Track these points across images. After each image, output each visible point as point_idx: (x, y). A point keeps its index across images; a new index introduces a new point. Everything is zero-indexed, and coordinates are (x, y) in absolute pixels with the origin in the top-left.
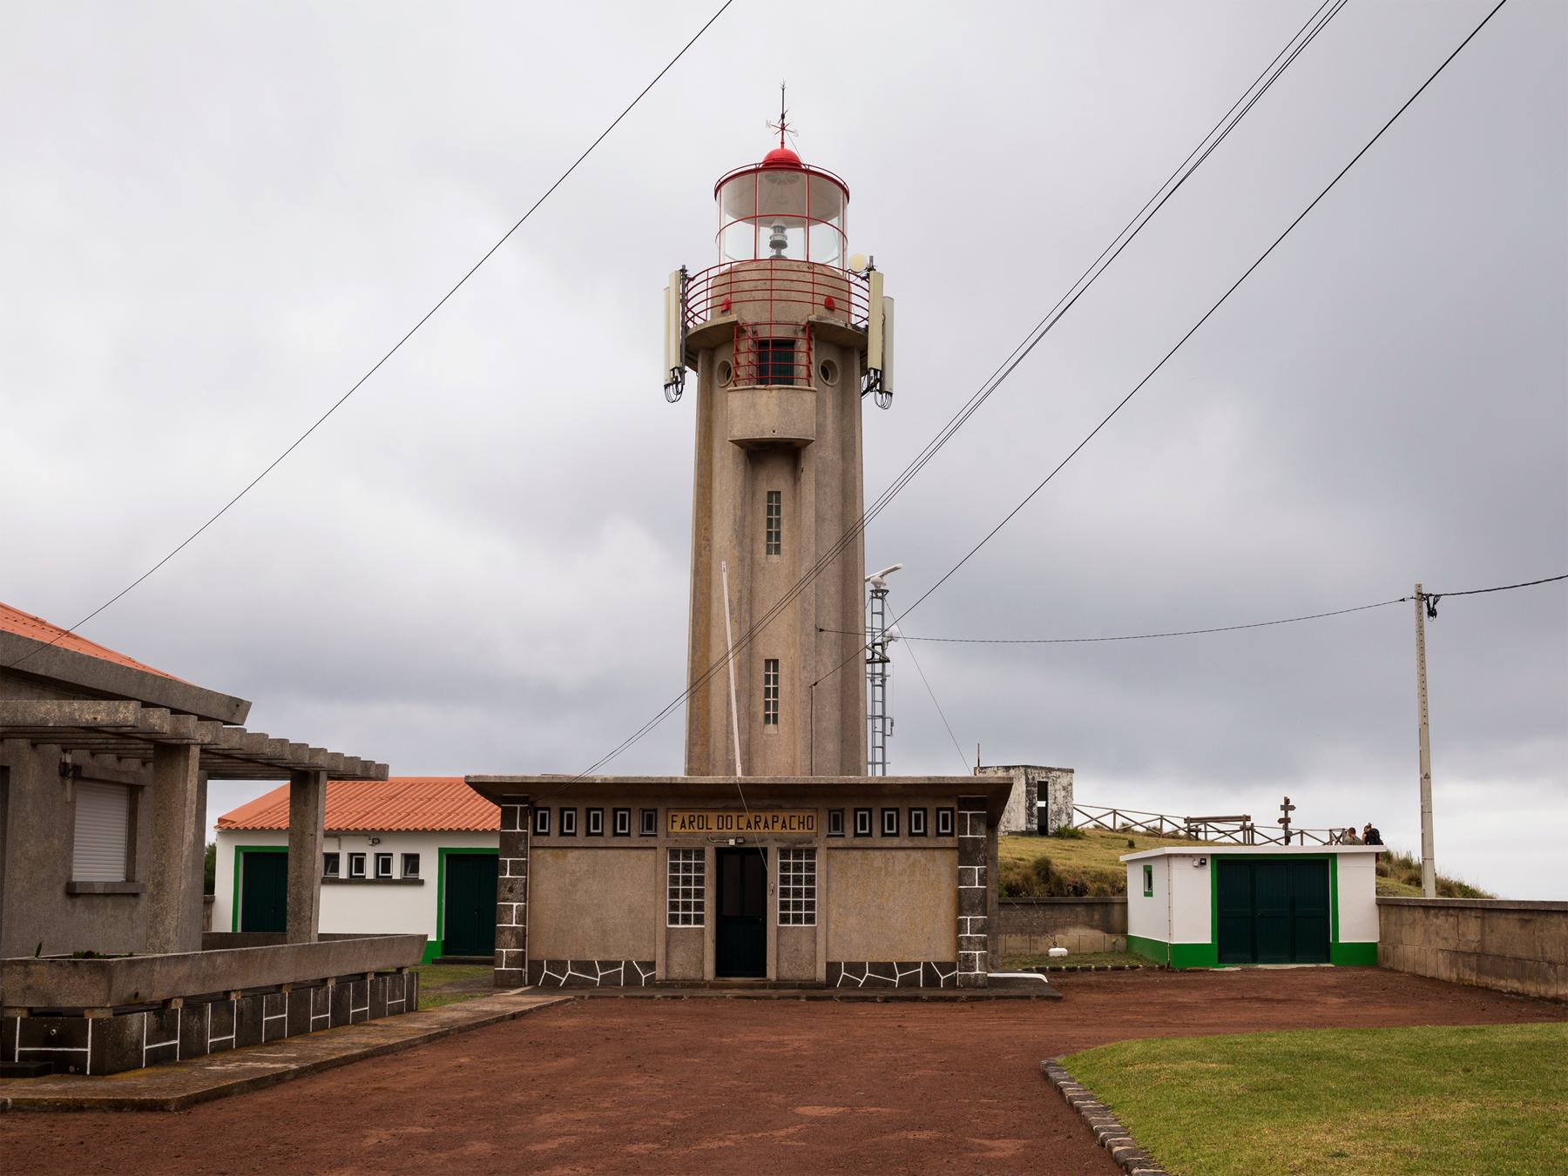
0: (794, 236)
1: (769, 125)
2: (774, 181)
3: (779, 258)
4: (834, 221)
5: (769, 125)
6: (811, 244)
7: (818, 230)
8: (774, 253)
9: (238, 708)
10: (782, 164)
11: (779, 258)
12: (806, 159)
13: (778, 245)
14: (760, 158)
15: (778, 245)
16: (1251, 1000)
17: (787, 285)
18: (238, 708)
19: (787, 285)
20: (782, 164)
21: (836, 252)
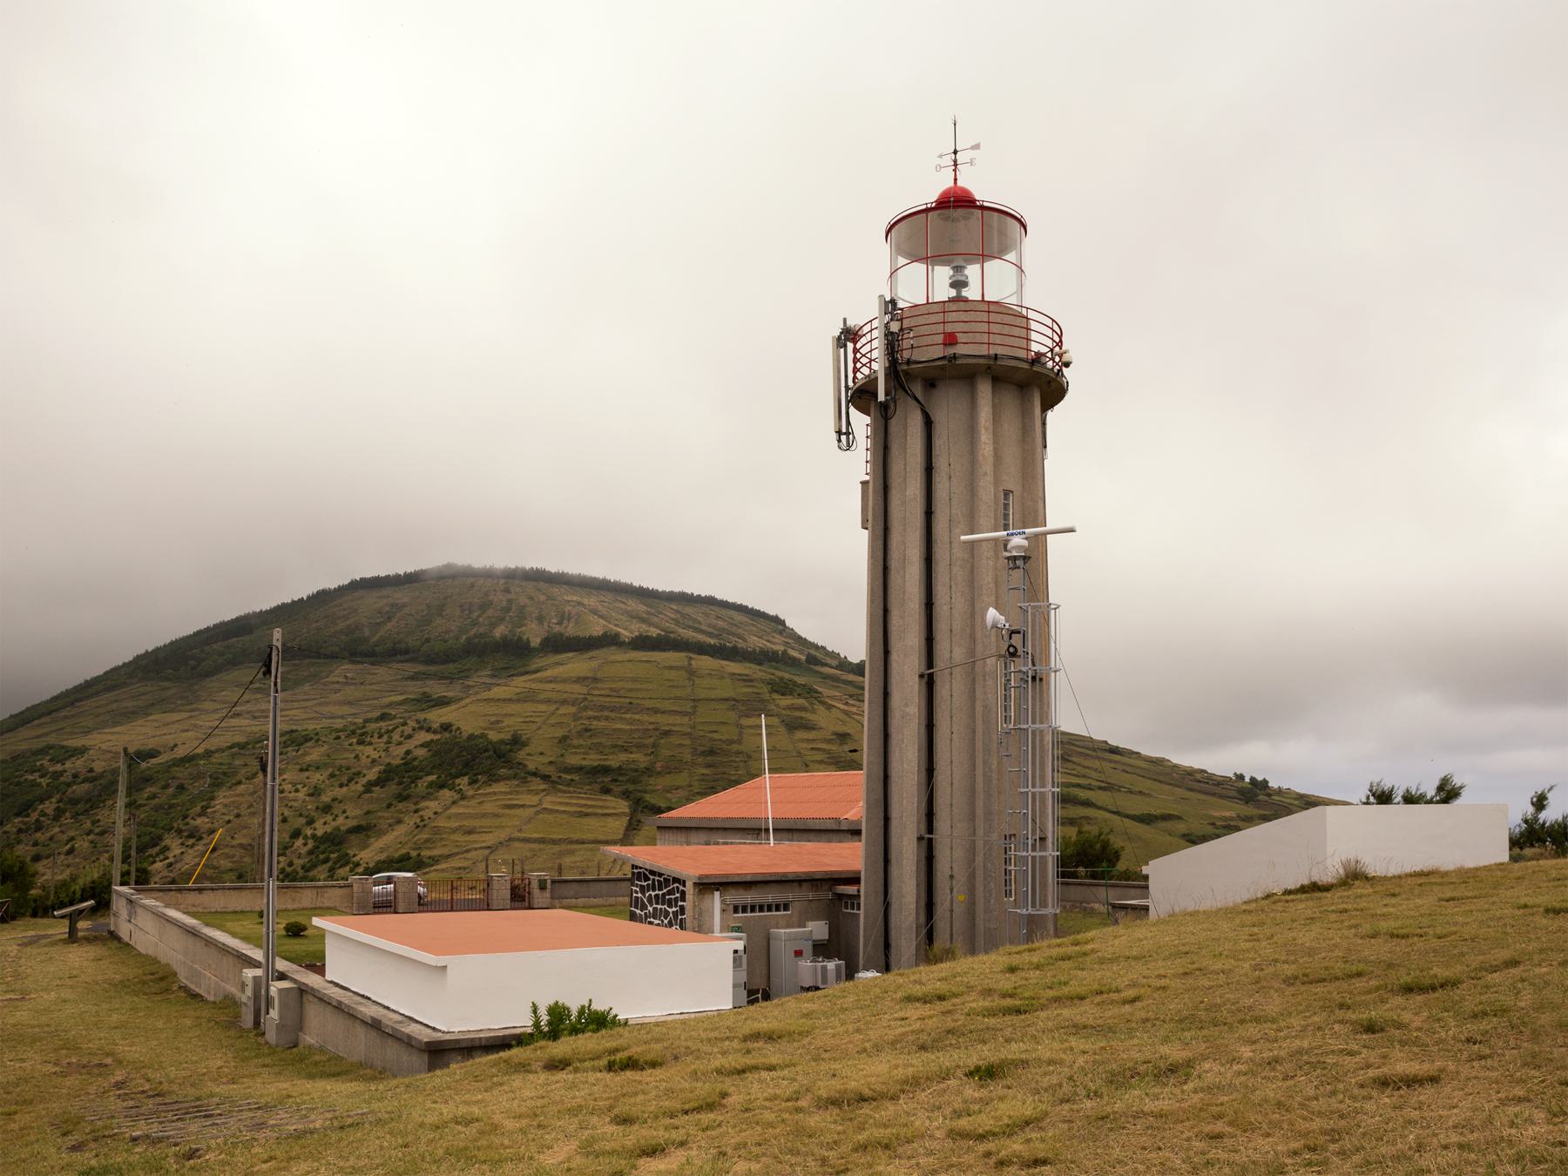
0: (972, 271)
1: (1540, 802)
2: (947, 219)
3: (959, 299)
4: (1012, 256)
5: (1540, 802)
6: (992, 281)
7: (992, 266)
8: (953, 293)
9: (864, 483)
10: (956, 202)
11: (959, 299)
12: (980, 195)
13: (958, 284)
14: (930, 197)
15: (958, 284)
16: (701, 649)
17: (1006, 330)
18: (864, 483)
19: (1006, 330)
20: (956, 202)
21: (1013, 287)
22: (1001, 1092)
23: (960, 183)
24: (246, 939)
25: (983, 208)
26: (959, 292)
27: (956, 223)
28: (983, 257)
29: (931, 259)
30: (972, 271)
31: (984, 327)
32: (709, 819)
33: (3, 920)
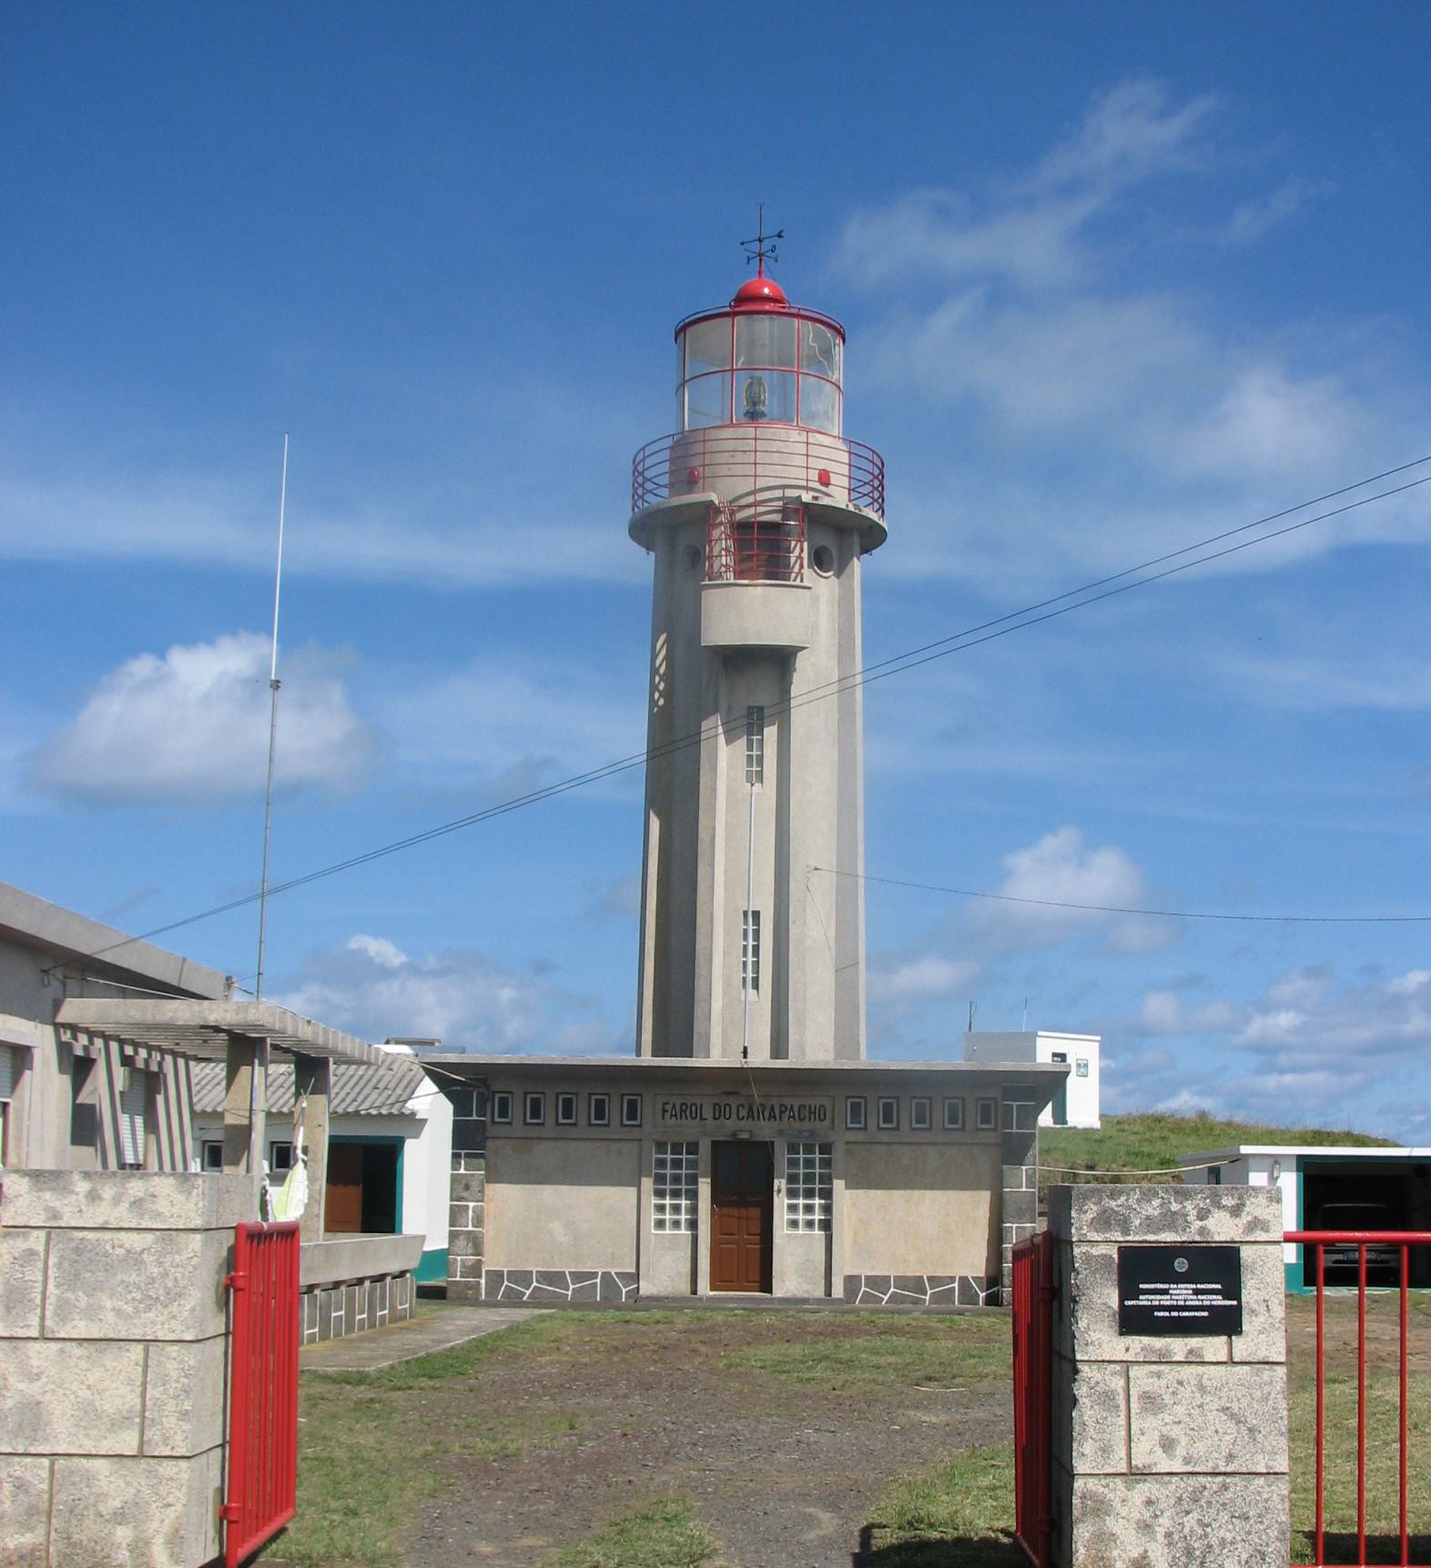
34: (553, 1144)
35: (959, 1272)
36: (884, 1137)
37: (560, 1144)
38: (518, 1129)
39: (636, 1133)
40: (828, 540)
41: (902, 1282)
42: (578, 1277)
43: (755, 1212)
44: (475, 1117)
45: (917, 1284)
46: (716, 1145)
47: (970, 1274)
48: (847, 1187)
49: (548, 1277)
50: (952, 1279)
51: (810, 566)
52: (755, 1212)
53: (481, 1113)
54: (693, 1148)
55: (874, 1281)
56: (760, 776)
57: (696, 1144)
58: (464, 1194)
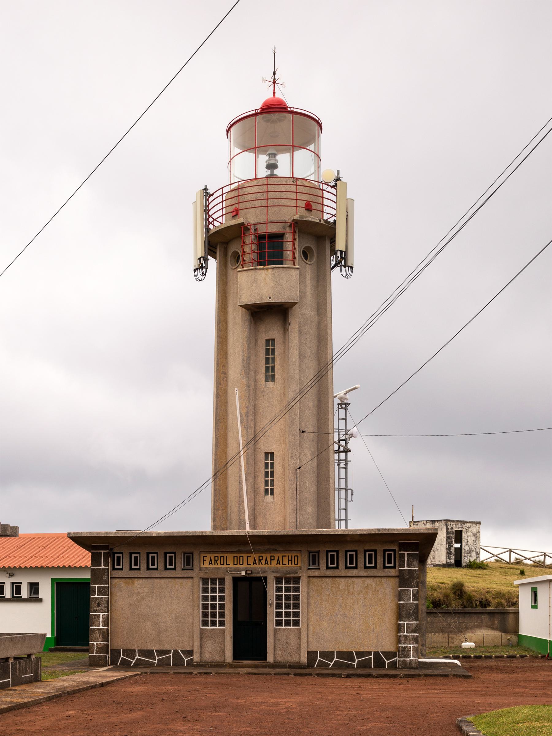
2: (268, 121)
3: (272, 176)
4: (312, 147)
7: (300, 154)
8: (269, 173)
10: (274, 108)
12: (292, 103)
13: (272, 166)
14: (258, 105)
15: (272, 166)
20: (274, 108)
21: (313, 169)
22: (79, 696)
23: (277, 95)
24: (241, 414)
25: (293, 113)
26: (272, 172)
27: (277, 123)
28: (293, 147)
29: (255, 149)
30: (263, 172)
31: (294, 196)
32: (386, 529)
33: (1, 714)
34: (144, 580)
35: (373, 650)
36: (329, 573)
37: (149, 580)
38: (126, 572)
39: (190, 573)
40: (311, 244)
41: (341, 654)
42: (160, 653)
43: (239, 619)
44: (103, 567)
45: (348, 656)
46: (236, 581)
47: (380, 650)
48: (45, 634)
49: (143, 653)
50: (369, 653)
51: (234, 146)
52: (239, 619)
53: (106, 564)
54: (222, 581)
55: (325, 654)
56: (273, 378)
57: (224, 579)
58: (98, 609)
